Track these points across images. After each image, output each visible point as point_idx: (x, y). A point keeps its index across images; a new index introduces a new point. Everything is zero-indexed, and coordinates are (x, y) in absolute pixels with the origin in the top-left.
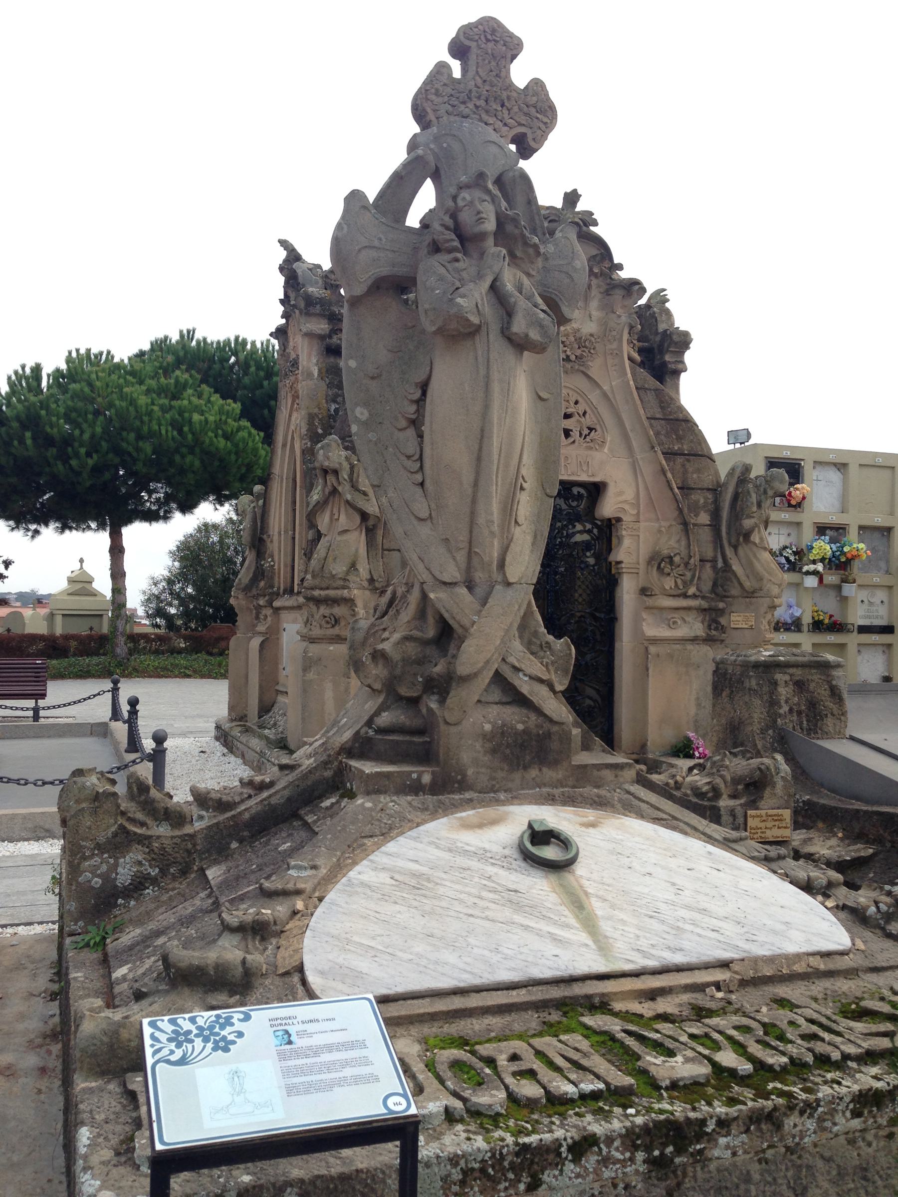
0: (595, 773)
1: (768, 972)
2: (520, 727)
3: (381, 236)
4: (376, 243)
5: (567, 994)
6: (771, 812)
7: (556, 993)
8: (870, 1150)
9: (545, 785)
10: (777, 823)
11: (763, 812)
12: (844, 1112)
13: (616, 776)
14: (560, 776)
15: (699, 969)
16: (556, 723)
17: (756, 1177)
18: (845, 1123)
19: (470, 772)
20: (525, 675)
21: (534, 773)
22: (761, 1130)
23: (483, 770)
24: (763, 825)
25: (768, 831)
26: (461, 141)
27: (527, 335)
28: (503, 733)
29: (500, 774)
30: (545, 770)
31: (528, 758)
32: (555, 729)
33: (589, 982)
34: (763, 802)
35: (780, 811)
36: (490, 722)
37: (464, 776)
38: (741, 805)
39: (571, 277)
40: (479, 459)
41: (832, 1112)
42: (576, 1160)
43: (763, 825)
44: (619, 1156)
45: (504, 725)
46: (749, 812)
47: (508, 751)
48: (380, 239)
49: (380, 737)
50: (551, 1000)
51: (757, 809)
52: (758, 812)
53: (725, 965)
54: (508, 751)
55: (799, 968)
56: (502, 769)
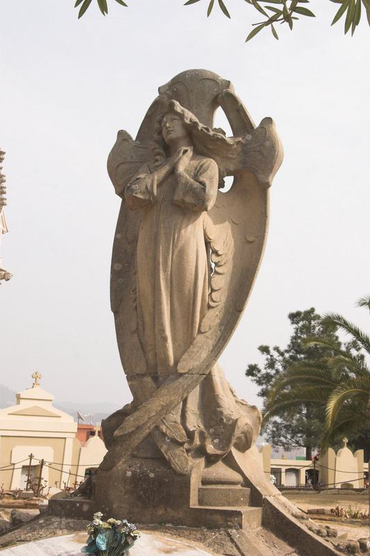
20: (168, 439)
27: (183, 200)
30: (169, 510)
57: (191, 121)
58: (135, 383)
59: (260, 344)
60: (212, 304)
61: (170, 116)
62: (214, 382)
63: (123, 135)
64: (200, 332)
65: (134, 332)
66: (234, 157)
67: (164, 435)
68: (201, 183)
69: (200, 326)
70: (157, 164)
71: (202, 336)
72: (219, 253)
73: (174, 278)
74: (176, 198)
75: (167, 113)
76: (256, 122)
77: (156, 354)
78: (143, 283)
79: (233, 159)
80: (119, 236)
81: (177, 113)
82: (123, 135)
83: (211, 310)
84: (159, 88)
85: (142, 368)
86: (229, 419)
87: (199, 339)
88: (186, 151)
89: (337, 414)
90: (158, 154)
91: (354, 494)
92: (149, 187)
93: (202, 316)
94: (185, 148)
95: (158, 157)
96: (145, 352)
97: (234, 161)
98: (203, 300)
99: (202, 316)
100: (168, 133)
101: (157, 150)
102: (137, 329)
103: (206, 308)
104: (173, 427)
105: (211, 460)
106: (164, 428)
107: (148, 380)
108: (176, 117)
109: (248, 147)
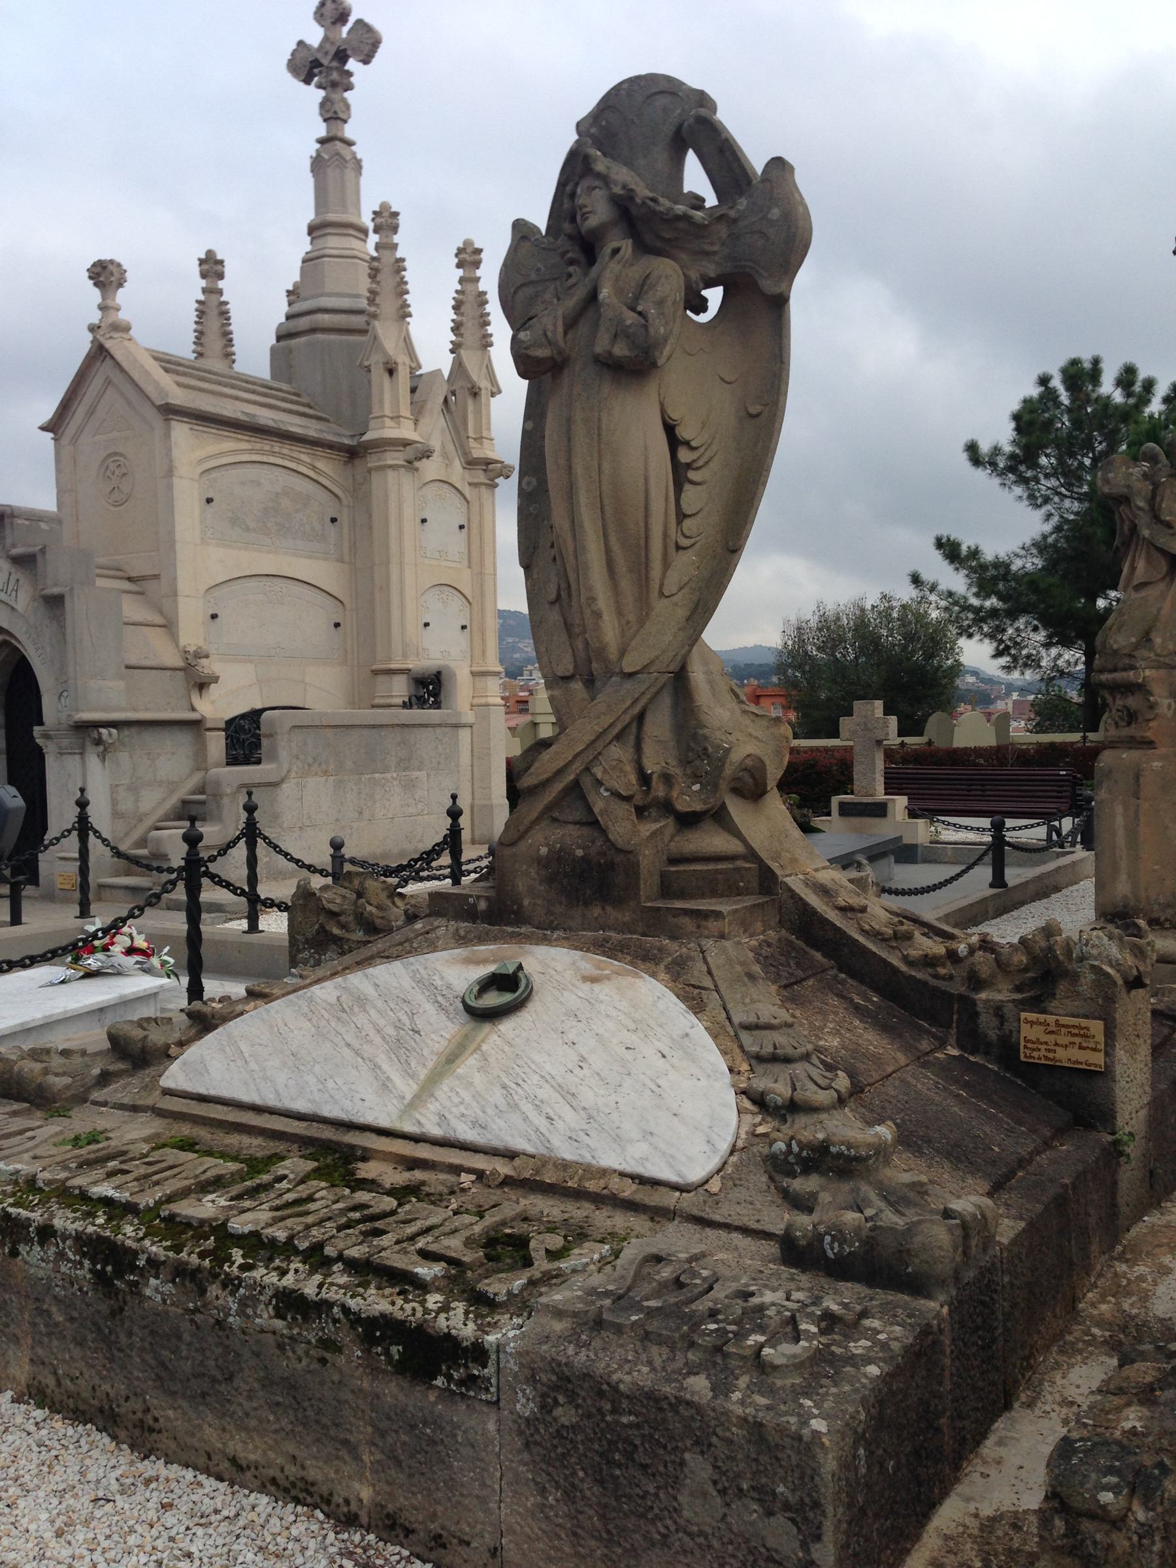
0: (671, 919)
1: (549, 1177)
2: (580, 853)
3: (539, 265)
4: (533, 277)
5: (334, 1138)
6: (1065, 1020)
7: (328, 1133)
8: (299, 1367)
9: (610, 929)
10: (1077, 1040)
11: (1051, 1019)
12: (267, 1305)
13: (699, 927)
14: (627, 919)
15: (486, 1153)
16: (620, 851)
17: (186, 1337)
18: (265, 1317)
19: (526, 902)
20: (607, 790)
21: (596, 911)
22: (183, 1285)
23: (540, 902)
24: (1051, 1038)
25: (1059, 1050)
26: (662, 92)
27: (610, 353)
28: (559, 859)
29: (559, 909)
30: (609, 909)
31: (589, 892)
32: (619, 858)
33: (368, 1134)
34: (1055, 1003)
35: (1084, 1022)
36: (548, 845)
37: (521, 906)
38: (1014, 1001)
39: (764, 235)
40: (573, 522)
41: (255, 1301)
42: (41, 1244)
43: (1044, 1038)
44: (71, 1255)
45: (560, 850)
46: (1023, 1015)
47: (565, 882)
48: (538, 270)
49: (672, 869)
50: (317, 1139)
51: (1044, 1012)
52: (1042, 1017)
53: (510, 1155)
54: (565, 882)
55: (592, 1186)
56: (560, 903)
57: (624, 187)
58: (557, 693)
59: (944, 532)
60: (684, 542)
61: (587, 182)
62: (693, 683)
63: (521, 229)
64: (662, 594)
65: (552, 603)
66: (715, 248)
67: (599, 783)
68: (640, 313)
69: (662, 585)
70: (572, 281)
71: (665, 601)
72: (693, 444)
73: (606, 501)
74: (598, 349)
75: (582, 177)
76: (758, 162)
77: (587, 643)
78: (559, 516)
79: (714, 253)
80: (530, 425)
81: (599, 176)
82: (521, 229)
83: (681, 552)
84: (578, 125)
85: (565, 666)
86: (719, 747)
87: (660, 607)
88: (616, 251)
89: (320, 972)
90: (572, 262)
91: (1032, 826)
92: (549, 334)
93: (666, 565)
94: (615, 244)
95: (571, 269)
96: (570, 635)
97: (716, 258)
98: (665, 536)
99: (666, 565)
100: (585, 217)
101: (570, 255)
102: (559, 596)
103: (672, 549)
104: (613, 768)
105: (688, 821)
106: (598, 771)
107: (577, 686)
108: (597, 183)
109: (741, 224)
